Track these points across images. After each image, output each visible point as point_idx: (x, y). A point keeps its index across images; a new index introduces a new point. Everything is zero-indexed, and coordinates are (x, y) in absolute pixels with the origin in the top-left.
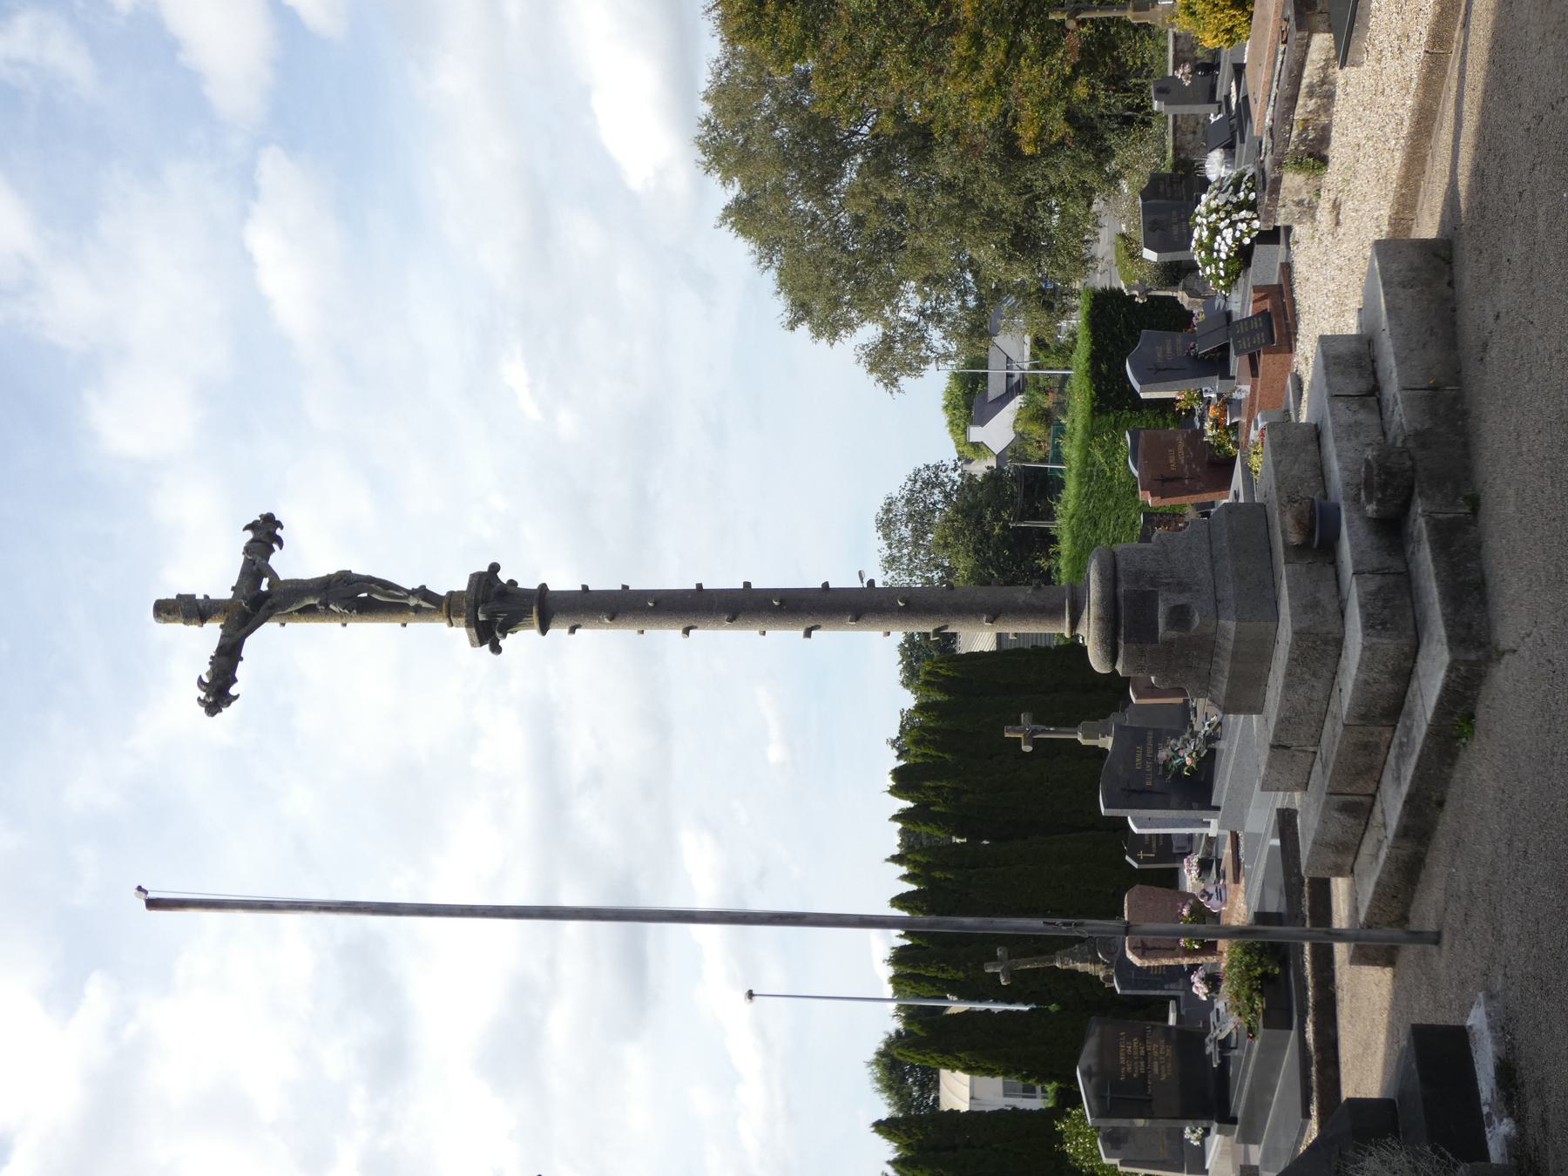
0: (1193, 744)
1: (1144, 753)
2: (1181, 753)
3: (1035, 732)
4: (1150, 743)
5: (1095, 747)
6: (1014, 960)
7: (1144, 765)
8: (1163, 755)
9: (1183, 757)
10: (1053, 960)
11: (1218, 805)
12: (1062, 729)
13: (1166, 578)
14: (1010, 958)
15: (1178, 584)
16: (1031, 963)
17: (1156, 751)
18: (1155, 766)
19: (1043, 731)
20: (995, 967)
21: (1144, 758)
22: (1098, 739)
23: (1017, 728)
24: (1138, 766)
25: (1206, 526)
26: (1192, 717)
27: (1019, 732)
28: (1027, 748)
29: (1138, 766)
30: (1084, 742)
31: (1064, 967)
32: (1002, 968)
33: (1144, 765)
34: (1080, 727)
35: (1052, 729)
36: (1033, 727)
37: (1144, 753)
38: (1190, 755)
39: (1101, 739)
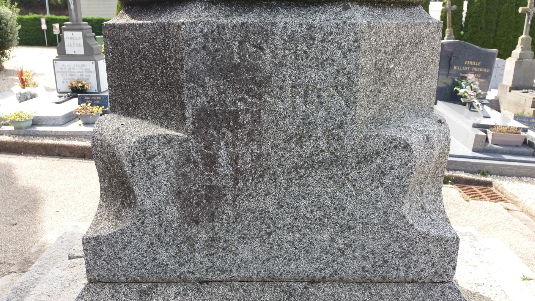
0: (472, 94)
1: (475, 66)
2: (468, 87)
3: (529, 14)
4: (481, 70)
5: (517, 44)
6: (451, 12)
7: (467, 66)
8: (471, 77)
9: (465, 88)
10: (449, 27)
11: (437, 104)
12: (529, 28)
13: (235, 159)
14: (452, 11)
15: (211, 188)
16: (449, 19)
17: (475, 73)
18: (466, 72)
19: (529, 18)
20: (449, 4)
21: (471, 66)
22: (521, 45)
23: (533, 5)
24: (467, 62)
25: (428, 274)
26: (524, 90)
27: (530, 5)
28: (520, 10)
29: (467, 62)
30: (520, 39)
31: (446, 32)
32: (448, 8)
33: (467, 66)
34: (529, 37)
35: (529, 23)
36: (532, 13)
37: (475, 66)
38: (466, 92)
39: (520, 46)
